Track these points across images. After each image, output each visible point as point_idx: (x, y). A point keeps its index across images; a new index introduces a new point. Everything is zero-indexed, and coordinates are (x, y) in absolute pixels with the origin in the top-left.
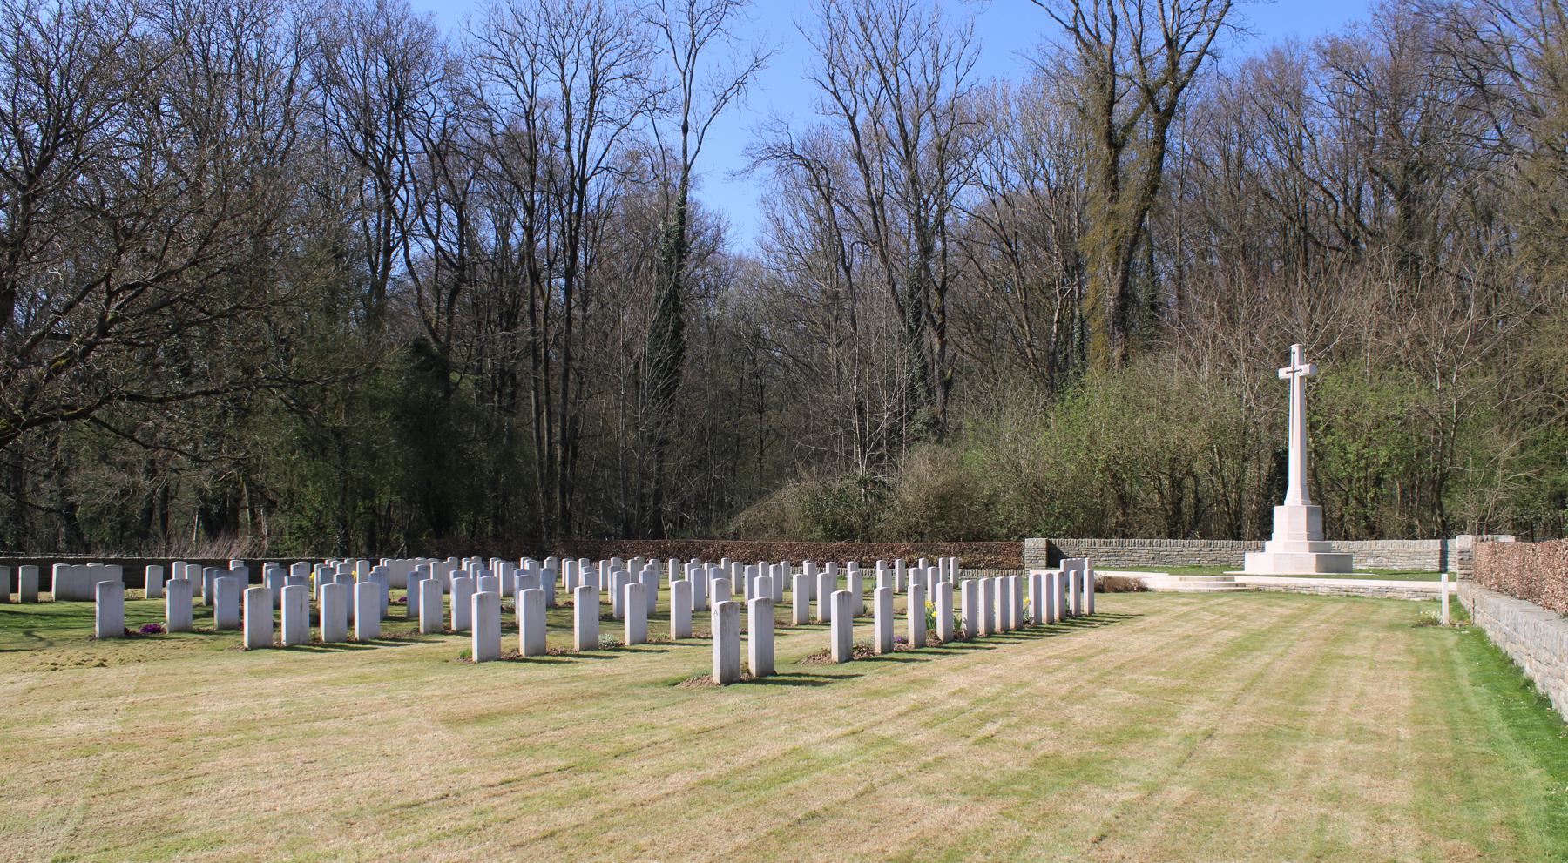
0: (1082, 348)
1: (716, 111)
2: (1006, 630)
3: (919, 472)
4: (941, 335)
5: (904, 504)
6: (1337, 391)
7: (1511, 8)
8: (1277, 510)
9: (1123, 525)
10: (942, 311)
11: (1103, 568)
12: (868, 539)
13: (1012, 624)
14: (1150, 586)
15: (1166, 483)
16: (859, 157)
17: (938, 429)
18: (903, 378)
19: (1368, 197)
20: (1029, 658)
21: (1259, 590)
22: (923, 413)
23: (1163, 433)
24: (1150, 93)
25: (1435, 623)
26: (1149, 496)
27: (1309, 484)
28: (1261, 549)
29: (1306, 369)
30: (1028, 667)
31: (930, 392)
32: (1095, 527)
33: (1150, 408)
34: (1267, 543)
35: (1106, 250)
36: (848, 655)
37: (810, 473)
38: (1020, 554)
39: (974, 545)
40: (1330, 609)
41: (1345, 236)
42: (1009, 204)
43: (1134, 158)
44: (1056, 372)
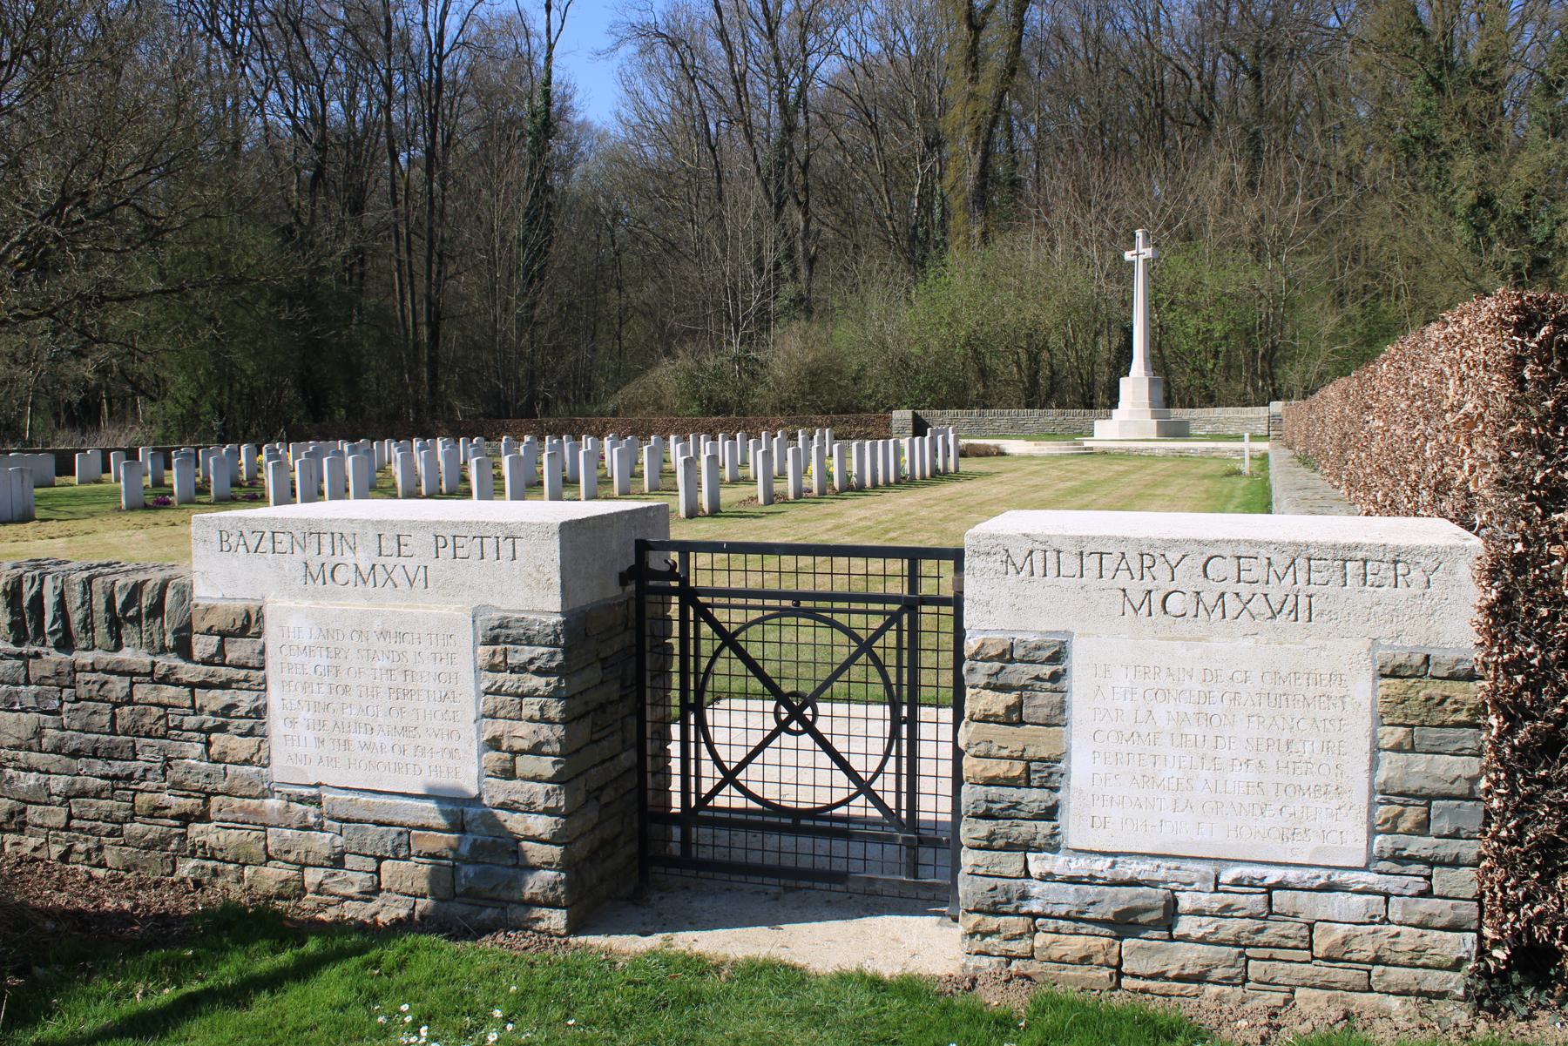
2: (887, 484)
3: (789, 350)
4: (805, 214)
5: (777, 381)
9: (984, 396)
10: (806, 188)
11: (966, 437)
13: (892, 479)
15: (1024, 357)
16: (722, 34)
17: (804, 305)
18: (769, 260)
19: (1223, 76)
20: (909, 500)
21: (1105, 453)
22: (788, 290)
23: (1019, 310)
25: (1239, 473)
26: (1007, 368)
27: (1153, 357)
28: (1109, 416)
29: (1148, 252)
30: (911, 505)
31: (795, 270)
32: (957, 398)
33: (1009, 286)
34: (1114, 411)
35: (967, 129)
36: (771, 498)
37: (685, 351)
38: (888, 425)
39: (845, 417)
40: (1160, 466)
41: (1200, 115)
42: (869, 75)
43: (995, 38)
44: (918, 248)
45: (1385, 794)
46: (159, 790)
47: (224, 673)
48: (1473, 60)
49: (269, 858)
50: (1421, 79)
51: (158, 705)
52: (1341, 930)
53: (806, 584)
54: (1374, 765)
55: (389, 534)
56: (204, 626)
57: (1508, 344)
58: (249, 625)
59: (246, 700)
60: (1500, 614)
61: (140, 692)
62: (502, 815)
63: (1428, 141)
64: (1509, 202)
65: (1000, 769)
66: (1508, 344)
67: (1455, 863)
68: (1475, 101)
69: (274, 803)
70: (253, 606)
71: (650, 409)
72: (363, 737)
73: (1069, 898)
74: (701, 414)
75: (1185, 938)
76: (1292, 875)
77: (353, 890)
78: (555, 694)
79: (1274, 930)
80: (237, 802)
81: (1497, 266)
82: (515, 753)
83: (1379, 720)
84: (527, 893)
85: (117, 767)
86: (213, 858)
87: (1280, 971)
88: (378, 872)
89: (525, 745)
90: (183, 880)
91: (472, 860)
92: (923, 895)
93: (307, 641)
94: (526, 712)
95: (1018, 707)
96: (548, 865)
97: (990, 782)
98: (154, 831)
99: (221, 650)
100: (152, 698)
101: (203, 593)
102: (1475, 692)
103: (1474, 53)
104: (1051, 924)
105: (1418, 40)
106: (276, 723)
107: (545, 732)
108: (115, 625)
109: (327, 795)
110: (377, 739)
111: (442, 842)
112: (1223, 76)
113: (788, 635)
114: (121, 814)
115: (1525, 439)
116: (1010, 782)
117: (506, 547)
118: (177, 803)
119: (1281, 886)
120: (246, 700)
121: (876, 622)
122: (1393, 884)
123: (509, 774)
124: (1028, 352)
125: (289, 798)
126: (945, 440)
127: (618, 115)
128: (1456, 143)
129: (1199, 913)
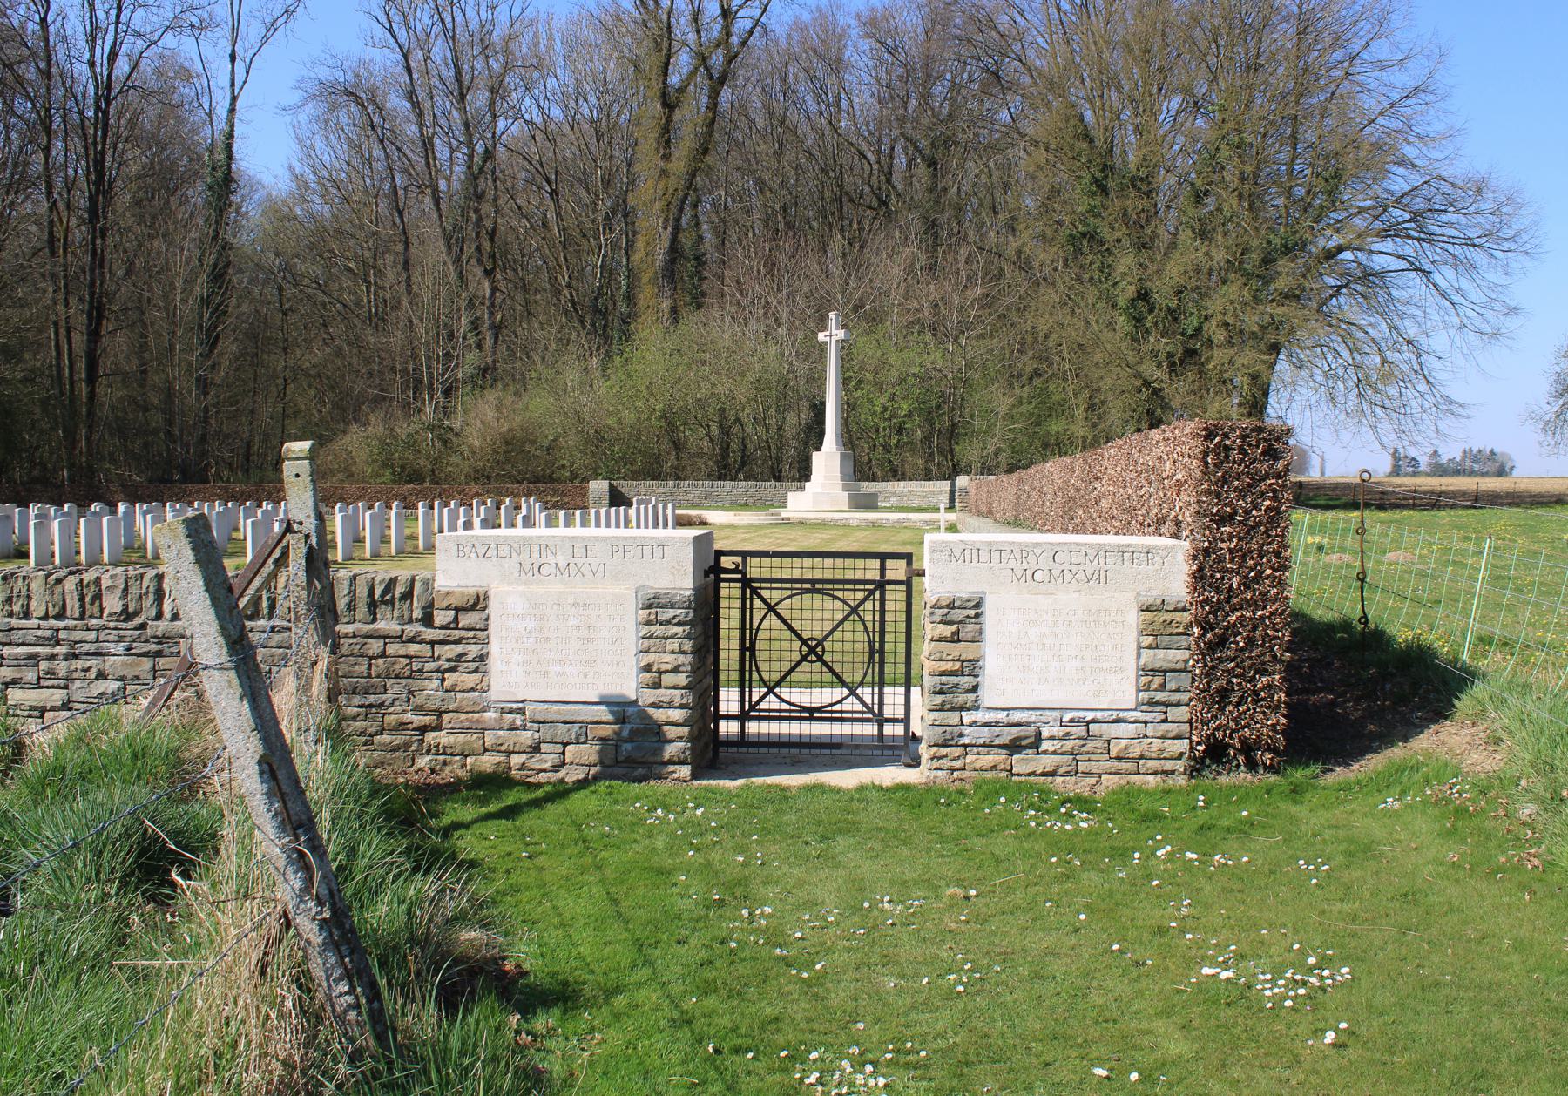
0: (630, 298)
1: (265, 40)
3: (481, 420)
6: (868, 349)
7: (1026, 8)
8: (815, 455)
9: (677, 468)
12: (436, 481)
14: (710, 520)
15: (715, 429)
16: (411, 95)
19: (901, 161)
21: (801, 523)
24: (703, 58)
26: (697, 439)
27: (1543, 496)
29: (841, 334)
32: (652, 471)
35: (658, 205)
38: (585, 495)
39: (541, 487)
45: (1146, 671)
46: (404, 712)
47: (457, 634)
48: (1132, 166)
49: (486, 750)
50: (1087, 179)
51: (406, 656)
52: (1124, 743)
53: (818, 575)
54: (1139, 656)
55: (580, 544)
56: (445, 604)
57: (1201, 445)
58: (478, 603)
59: (473, 650)
60: (1198, 577)
61: (390, 650)
62: (651, 711)
63: (1092, 236)
64: (1163, 297)
65: (948, 666)
66: (1201, 445)
67: (1178, 704)
68: (1134, 203)
69: (491, 715)
70: (482, 591)
71: (340, 476)
72: (558, 669)
73: (984, 734)
74: (394, 482)
75: (1045, 753)
76: (1099, 715)
77: (547, 766)
78: (688, 637)
79: (1090, 745)
80: (463, 716)
81: (1154, 354)
82: (660, 673)
83: (1141, 633)
84: (666, 757)
85: (372, 699)
86: (444, 753)
87: (1094, 767)
88: (563, 753)
89: (669, 667)
90: (421, 769)
91: (630, 740)
92: (887, 752)
93: (520, 611)
94: (669, 648)
95: (957, 632)
96: (680, 739)
97: (942, 674)
98: (399, 740)
99: (456, 620)
100: (401, 652)
101: (442, 583)
102: (1186, 617)
103: (1133, 158)
104: (975, 750)
105: (1085, 145)
106: (495, 664)
107: (682, 659)
108: (373, 605)
109: (529, 708)
110: (568, 669)
111: (606, 731)
112: (901, 161)
113: (807, 603)
114: (373, 730)
115: (1208, 492)
116: (953, 673)
117: (658, 552)
118: (418, 720)
119: (1094, 721)
120: (473, 650)
121: (860, 595)
122: (1148, 717)
123: (657, 685)
124: (721, 425)
125: (503, 711)
126: (665, 508)
127: (291, 168)
128: (1119, 241)
129: (1052, 738)
